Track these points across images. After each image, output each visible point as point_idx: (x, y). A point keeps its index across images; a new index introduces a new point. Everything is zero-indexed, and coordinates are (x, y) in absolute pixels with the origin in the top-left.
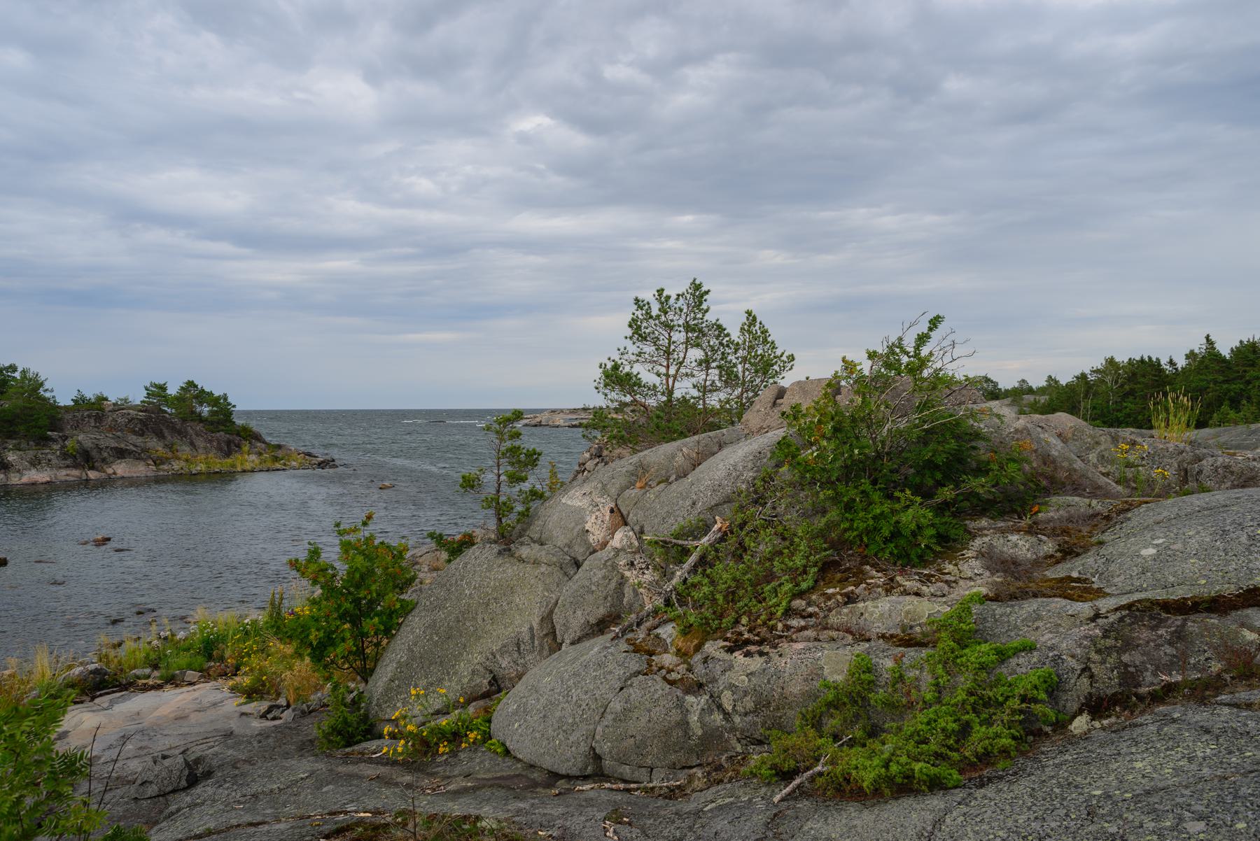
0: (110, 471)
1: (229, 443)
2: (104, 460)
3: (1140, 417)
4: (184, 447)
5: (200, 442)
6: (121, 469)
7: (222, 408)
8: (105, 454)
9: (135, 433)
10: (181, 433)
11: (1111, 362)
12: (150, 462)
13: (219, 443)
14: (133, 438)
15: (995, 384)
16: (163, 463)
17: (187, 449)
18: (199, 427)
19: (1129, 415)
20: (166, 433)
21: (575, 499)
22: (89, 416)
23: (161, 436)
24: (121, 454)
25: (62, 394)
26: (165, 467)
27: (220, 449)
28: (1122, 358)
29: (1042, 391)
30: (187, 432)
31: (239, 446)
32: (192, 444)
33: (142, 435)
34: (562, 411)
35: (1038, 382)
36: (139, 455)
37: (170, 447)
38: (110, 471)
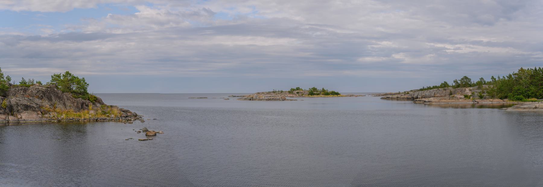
0: (19, 116)
1: (82, 104)
2: (18, 111)
3: (537, 94)
4: (60, 106)
5: (68, 103)
6: (25, 116)
7: (82, 84)
8: (19, 108)
9: (38, 98)
10: (59, 98)
11: (522, 70)
12: (40, 113)
13: (78, 104)
14: (37, 101)
15: (470, 80)
16: (46, 114)
17: (61, 106)
18: (70, 95)
19: (532, 93)
20: (53, 98)
21: (10, 118)
22: (21, 90)
23: (50, 99)
24: (27, 108)
25: (16, 81)
26: (46, 116)
27: (77, 107)
28: (525, 68)
29: (489, 83)
30: (63, 97)
31: (87, 106)
32: (64, 104)
33: (42, 99)
34: (263, 93)
35: (488, 79)
36: (39, 109)
37: (53, 105)
38: (19, 116)
